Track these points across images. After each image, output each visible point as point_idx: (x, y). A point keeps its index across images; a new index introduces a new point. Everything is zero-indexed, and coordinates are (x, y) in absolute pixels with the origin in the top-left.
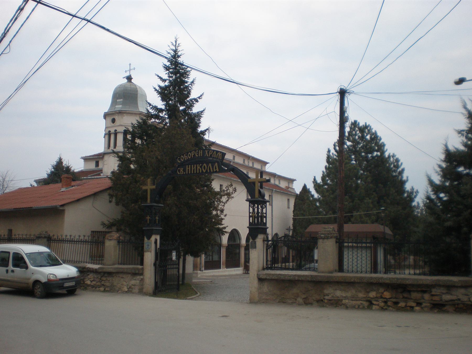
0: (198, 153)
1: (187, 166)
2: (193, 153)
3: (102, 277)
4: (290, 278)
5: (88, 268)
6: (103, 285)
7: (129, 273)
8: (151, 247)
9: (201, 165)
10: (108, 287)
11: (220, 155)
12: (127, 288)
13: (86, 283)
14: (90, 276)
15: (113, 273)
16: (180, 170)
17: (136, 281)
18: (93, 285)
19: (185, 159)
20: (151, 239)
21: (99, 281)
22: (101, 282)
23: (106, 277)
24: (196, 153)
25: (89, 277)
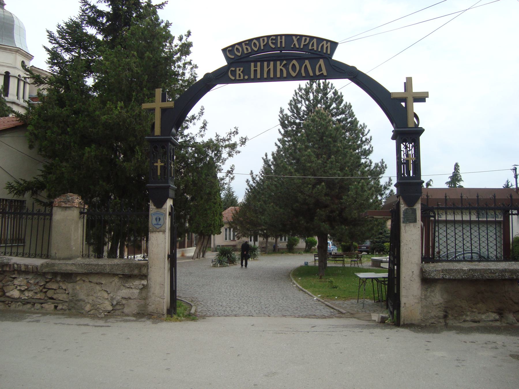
0: (274, 41)
1: (252, 64)
2: (305, 41)
3: (47, 282)
4: (494, 275)
5: (16, 266)
6: (52, 298)
7: (115, 275)
8: (165, 223)
9: (285, 62)
10: (63, 302)
11: (327, 47)
12: (112, 305)
13: (7, 294)
14: (19, 280)
15: (77, 274)
16: (235, 71)
17: (131, 291)
18: (26, 298)
19: (246, 52)
20: (164, 207)
21: (41, 291)
22: (46, 292)
23: (58, 282)
24: (270, 42)
25: (16, 282)
